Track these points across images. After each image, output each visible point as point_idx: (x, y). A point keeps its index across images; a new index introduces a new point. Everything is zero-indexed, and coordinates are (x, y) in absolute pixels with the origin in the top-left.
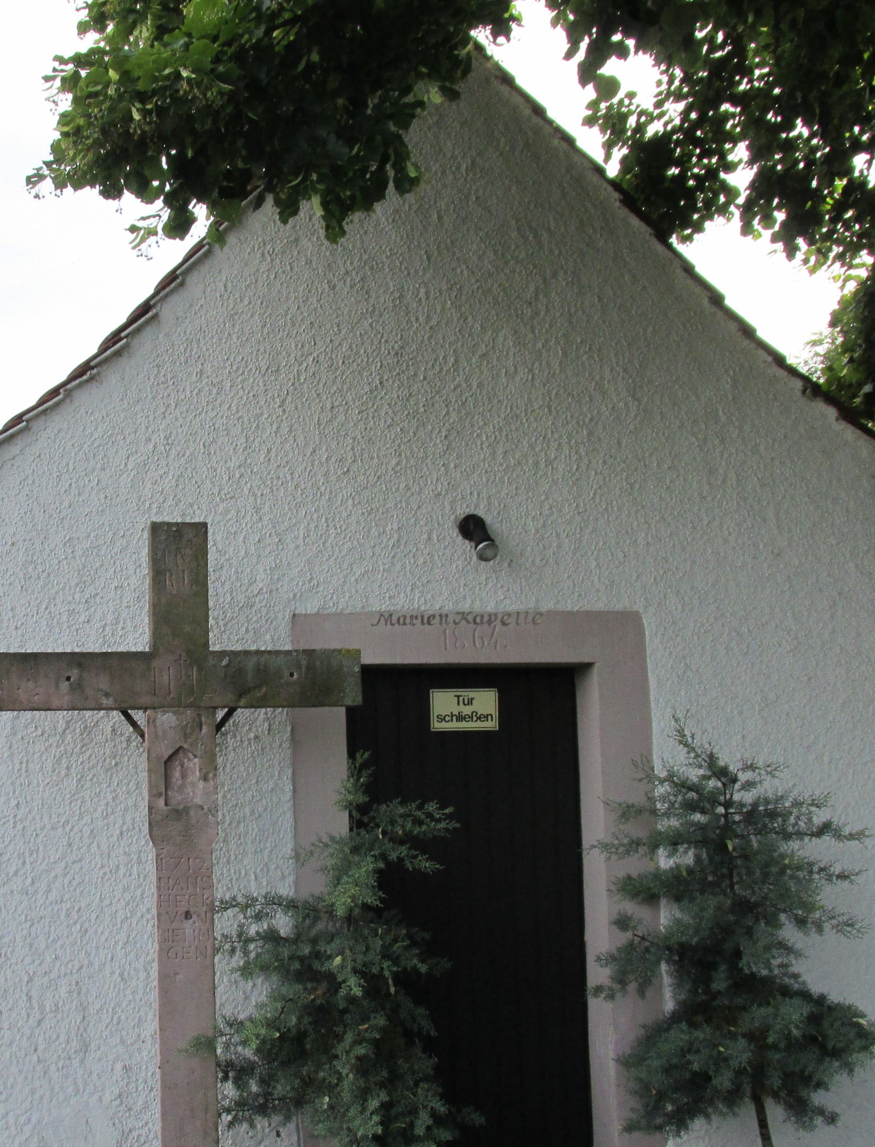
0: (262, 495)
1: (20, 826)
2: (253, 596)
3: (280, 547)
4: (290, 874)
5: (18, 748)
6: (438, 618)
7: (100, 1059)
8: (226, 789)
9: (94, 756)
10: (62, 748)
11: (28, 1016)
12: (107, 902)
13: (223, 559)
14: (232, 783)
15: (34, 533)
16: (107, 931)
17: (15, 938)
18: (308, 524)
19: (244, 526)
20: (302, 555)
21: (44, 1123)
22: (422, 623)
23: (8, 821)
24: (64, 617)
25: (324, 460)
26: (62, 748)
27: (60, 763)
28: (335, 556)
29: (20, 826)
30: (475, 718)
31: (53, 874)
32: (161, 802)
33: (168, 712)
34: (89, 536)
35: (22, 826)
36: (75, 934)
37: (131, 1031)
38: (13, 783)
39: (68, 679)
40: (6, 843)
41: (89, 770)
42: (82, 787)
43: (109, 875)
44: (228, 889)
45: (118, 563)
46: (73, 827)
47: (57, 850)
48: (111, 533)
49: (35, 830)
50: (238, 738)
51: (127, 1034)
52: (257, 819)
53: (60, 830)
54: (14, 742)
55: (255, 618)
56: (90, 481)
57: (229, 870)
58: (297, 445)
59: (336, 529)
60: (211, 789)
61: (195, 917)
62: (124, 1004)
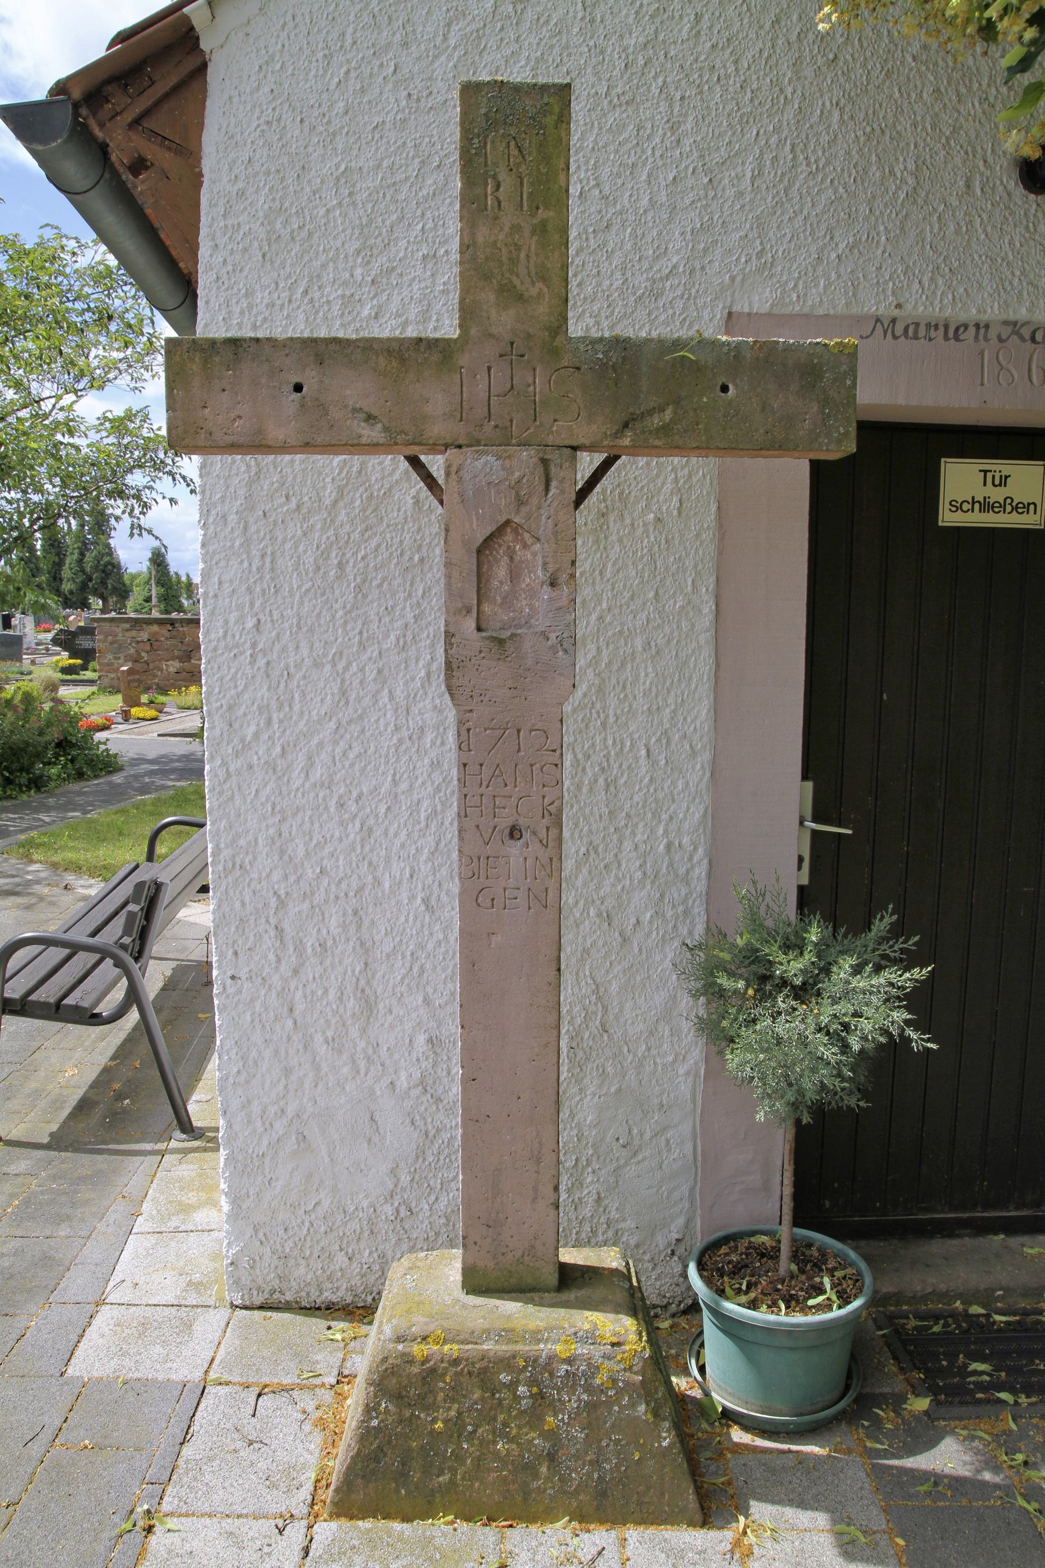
0: (682, 98)
1: (261, 662)
2: (661, 279)
3: (711, 194)
4: (704, 747)
5: (258, 531)
6: (972, 330)
7: (392, 1027)
8: (604, 605)
9: (384, 546)
10: (331, 532)
11: (279, 960)
12: (404, 786)
13: (611, 210)
14: (615, 597)
15: (285, 159)
16: (405, 832)
17: (256, 840)
18: (761, 154)
19: (650, 152)
20: (747, 208)
21: (305, 1117)
22: (946, 338)
23: (242, 653)
24: (336, 309)
25: (793, 37)
26: (331, 532)
27: (328, 558)
28: (805, 212)
29: (261, 662)
30: (1009, 508)
31: (315, 740)
32: (470, 624)
33: (486, 453)
34: (379, 166)
35: (264, 661)
36: (352, 836)
37: (440, 987)
38: (249, 590)
39: (298, 388)
40: (240, 688)
41: (376, 569)
42: (365, 596)
43: (408, 743)
44: (603, 769)
45: (428, 214)
46: (349, 664)
47: (322, 700)
48: (417, 161)
49: (287, 668)
50: (628, 521)
51: (435, 990)
52: (653, 657)
53: (328, 667)
54: (251, 520)
55: (662, 318)
56: (381, 65)
57: (605, 739)
58: (749, 10)
59: (808, 165)
60: (564, 601)
61: (527, 835)
62: (430, 946)
